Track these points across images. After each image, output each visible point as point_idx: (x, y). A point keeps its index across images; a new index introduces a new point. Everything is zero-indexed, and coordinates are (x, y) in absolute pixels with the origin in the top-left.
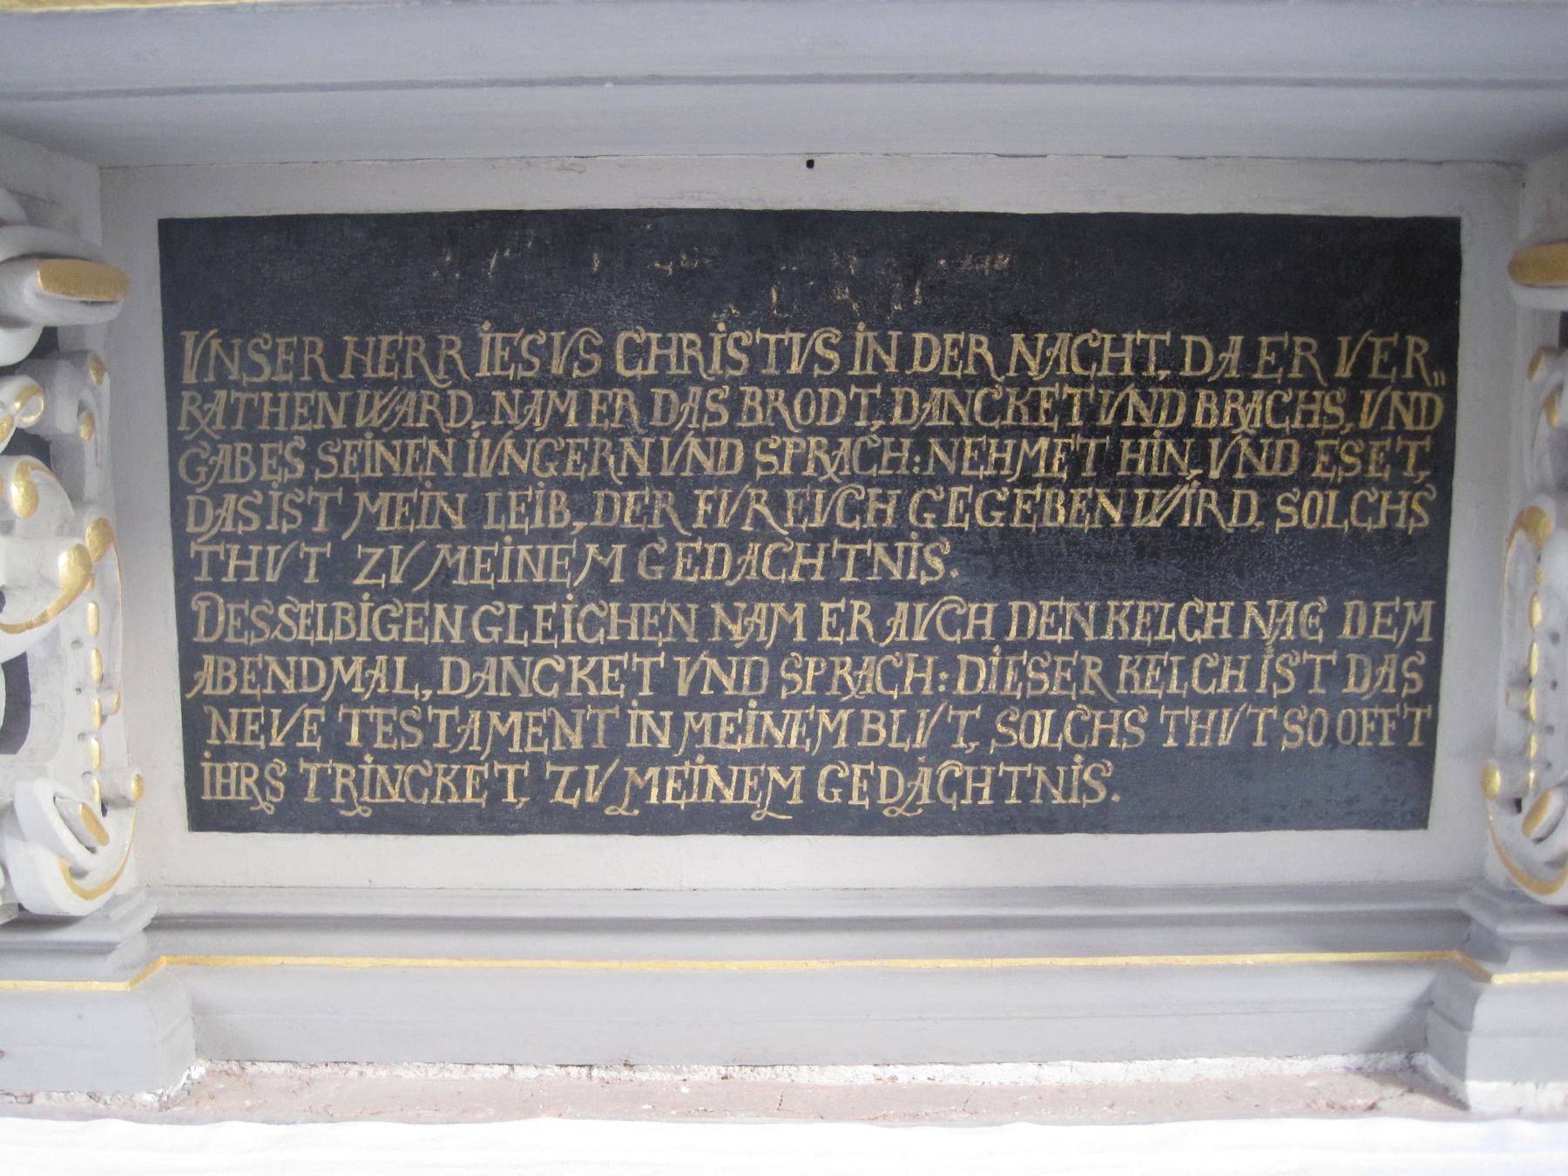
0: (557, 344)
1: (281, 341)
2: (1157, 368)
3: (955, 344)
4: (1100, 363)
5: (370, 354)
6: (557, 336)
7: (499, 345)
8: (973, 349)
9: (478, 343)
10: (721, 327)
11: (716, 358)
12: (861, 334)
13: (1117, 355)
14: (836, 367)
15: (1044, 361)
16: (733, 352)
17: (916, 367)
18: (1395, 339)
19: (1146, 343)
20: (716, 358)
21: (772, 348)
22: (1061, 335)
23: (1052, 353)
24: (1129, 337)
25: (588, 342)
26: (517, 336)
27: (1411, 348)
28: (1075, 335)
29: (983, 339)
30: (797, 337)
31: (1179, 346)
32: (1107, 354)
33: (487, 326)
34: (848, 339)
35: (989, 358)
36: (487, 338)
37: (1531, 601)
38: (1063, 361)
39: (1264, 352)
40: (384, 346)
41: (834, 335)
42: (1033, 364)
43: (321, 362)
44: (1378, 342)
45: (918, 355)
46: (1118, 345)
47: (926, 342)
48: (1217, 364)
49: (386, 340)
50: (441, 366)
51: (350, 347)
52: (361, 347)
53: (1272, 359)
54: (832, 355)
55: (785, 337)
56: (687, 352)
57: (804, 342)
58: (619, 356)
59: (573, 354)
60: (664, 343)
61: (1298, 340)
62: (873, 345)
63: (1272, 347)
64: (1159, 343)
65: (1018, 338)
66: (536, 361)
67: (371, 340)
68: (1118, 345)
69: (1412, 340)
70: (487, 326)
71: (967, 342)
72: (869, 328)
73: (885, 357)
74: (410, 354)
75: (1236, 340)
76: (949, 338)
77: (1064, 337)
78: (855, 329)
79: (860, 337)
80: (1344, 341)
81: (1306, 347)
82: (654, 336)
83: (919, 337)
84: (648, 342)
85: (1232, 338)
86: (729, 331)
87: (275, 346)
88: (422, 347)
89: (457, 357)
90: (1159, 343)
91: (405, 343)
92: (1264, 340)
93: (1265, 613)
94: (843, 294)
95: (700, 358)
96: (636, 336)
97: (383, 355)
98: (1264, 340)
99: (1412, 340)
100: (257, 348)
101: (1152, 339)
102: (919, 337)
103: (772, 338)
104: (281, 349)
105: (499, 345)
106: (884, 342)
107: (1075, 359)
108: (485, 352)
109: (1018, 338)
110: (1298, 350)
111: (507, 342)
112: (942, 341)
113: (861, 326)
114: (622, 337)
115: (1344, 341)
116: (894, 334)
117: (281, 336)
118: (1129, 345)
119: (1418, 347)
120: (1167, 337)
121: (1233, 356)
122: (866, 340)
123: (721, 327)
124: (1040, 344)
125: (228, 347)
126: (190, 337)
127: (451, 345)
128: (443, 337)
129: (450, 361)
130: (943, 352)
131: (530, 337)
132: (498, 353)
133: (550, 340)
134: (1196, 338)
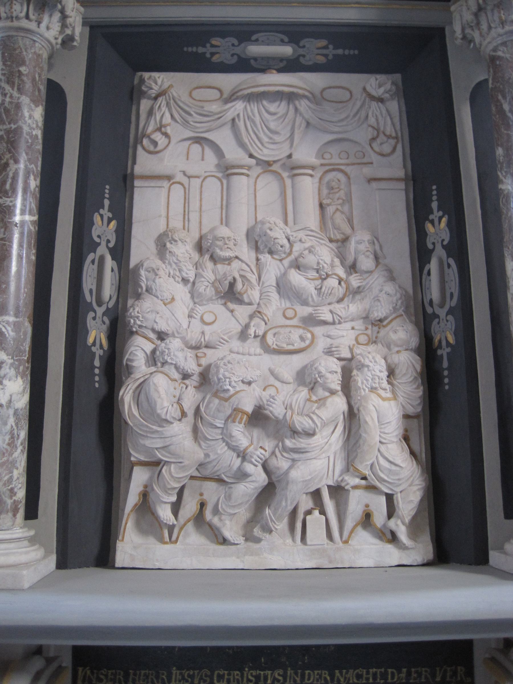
0: (196, 674)
1: (110, 672)
2: (380, 680)
3: (318, 674)
4: (362, 678)
5: (138, 676)
6: (196, 672)
7: (178, 674)
8: (323, 675)
9: (171, 673)
10: (247, 669)
11: (245, 679)
12: (290, 672)
13: (368, 676)
14: (282, 681)
15: (345, 678)
16: (250, 677)
17: (306, 681)
18: (454, 668)
19: (376, 672)
20: (245, 679)
21: (262, 676)
22: (350, 670)
23: (348, 676)
24: (371, 670)
25: (206, 674)
26: (184, 672)
27: (459, 670)
28: (355, 670)
29: (326, 672)
30: (270, 672)
31: (386, 673)
32: (365, 676)
33: (174, 668)
34: (285, 673)
35: (328, 678)
36: (174, 672)
37: (143, 138)
38: (351, 678)
39: (413, 673)
40: (142, 674)
41: (281, 672)
42: (342, 680)
43: (122, 678)
44: (449, 669)
45: (307, 677)
46: (368, 673)
47: (309, 674)
48: (399, 678)
49: (143, 672)
50: (160, 680)
51: (131, 674)
52: (135, 674)
53: (416, 675)
54: (280, 678)
55: (266, 672)
56: (236, 677)
57: (272, 674)
58: (215, 678)
59: (201, 678)
60: (229, 674)
61: (424, 669)
62: (293, 675)
63: (416, 672)
64: (381, 672)
65: (337, 671)
66: (190, 680)
67: (138, 672)
68: (368, 673)
69: (459, 668)
70: (174, 668)
71: (322, 673)
72: (292, 669)
73: (296, 678)
74: (150, 677)
75: (404, 670)
76: (316, 672)
77: (351, 671)
78: (287, 670)
79: (289, 672)
80: (438, 669)
81: (426, 671)
82: (226, 672)
83: (307, 672)
84: (224, 675)
85: (403, 669)
86: (249, 671)
87: (108, 673)
88: (154, 675)
89: (165, 678)
90: (381, 672)
91: (149, 673)
92: (413, 670)
93: (341, 674)
94: (283, 659)
95: (240, 679)
96: (220, 672)
97: (142, 677)
98: (413, 670)
99: (459, 668)
100: (102, 674)
101: (379, 671)
102: (307, 672)
103: (262, 673)
104: (110, 674)
105: (178, 674)
106: (296, 674)
107: (354, 678)
108: (174, 677)
109: (337, 671)
110: (424, 673)
111: (181, 674)
112: (314, 673)
113: (289, 669)
114: (216, 672)
115: (438, 669)
116: (299, 671)
117: (109, 670)
118: (371, 673)
119: (461, 670)
120: (383, 670)
121: (403, 675)
122: (291, 673)
123: (247, 669)
124: (344, 673)
125: (92, 673)
126: (80, 669)
127: (163, 674)
128: (161, 672)
129: (163, 679)
130: (314, 676)
131: (187, 672)
132: (178, 677)
133: (194, 673)
134: (392, 670)
